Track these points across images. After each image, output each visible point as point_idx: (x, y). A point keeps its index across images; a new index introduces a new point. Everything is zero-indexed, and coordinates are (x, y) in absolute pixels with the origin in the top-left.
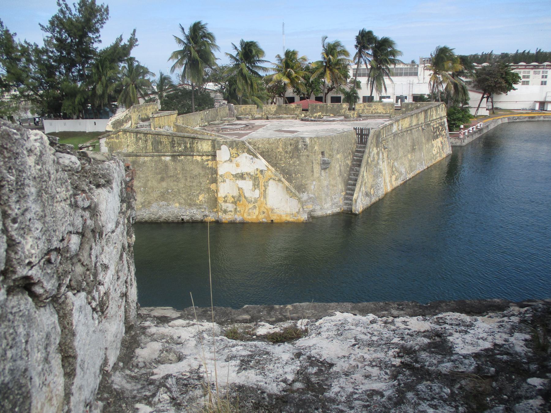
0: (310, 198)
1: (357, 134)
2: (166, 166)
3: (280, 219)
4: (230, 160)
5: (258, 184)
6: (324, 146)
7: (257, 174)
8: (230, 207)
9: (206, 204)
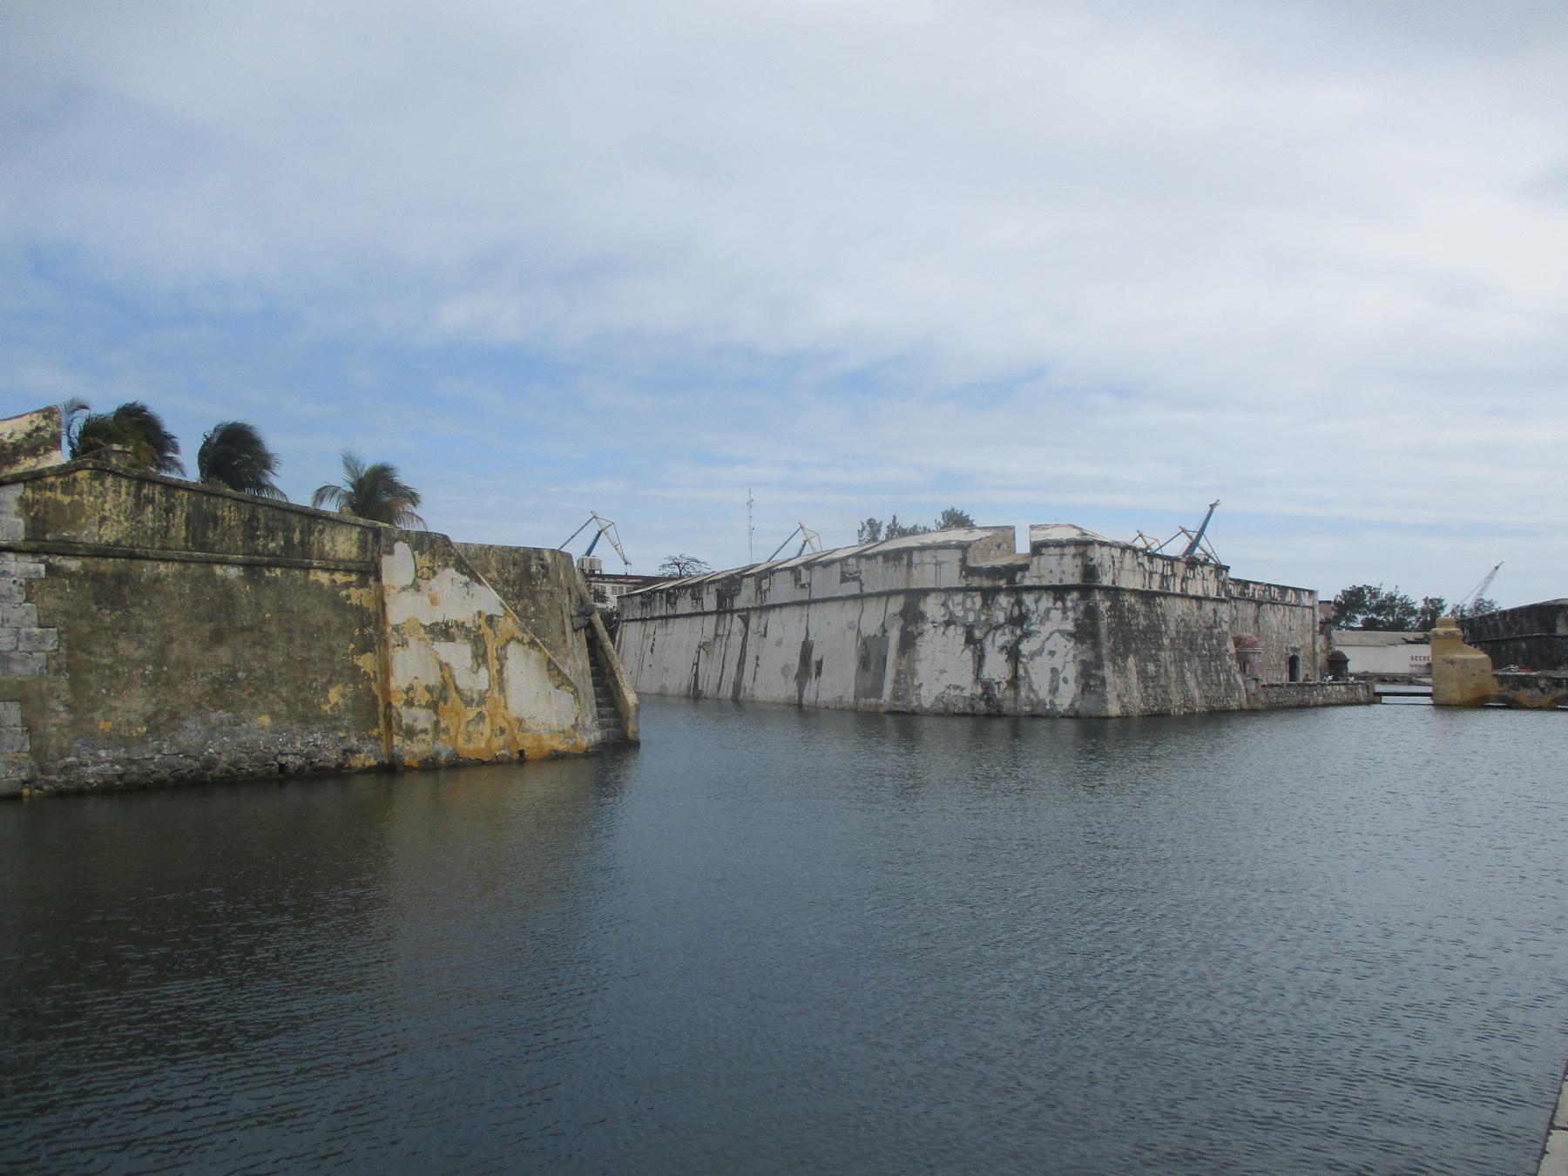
2: (228, 594)
4: (415, 586)
9: (349, 716)
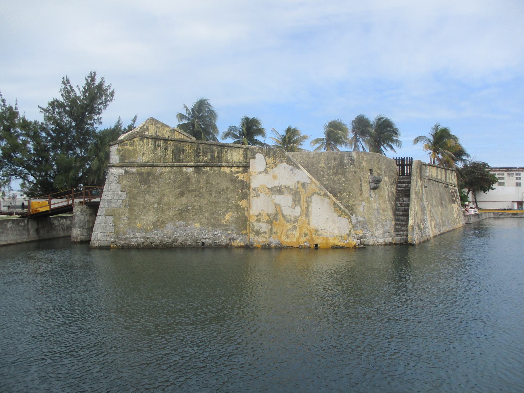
0: (359, 222)
1: (397, 165)
3: (327, 243)
4: (266, 171)
6: (373, 163)
7: (298, 188)
8: (264, 227)
9: (234, 225)
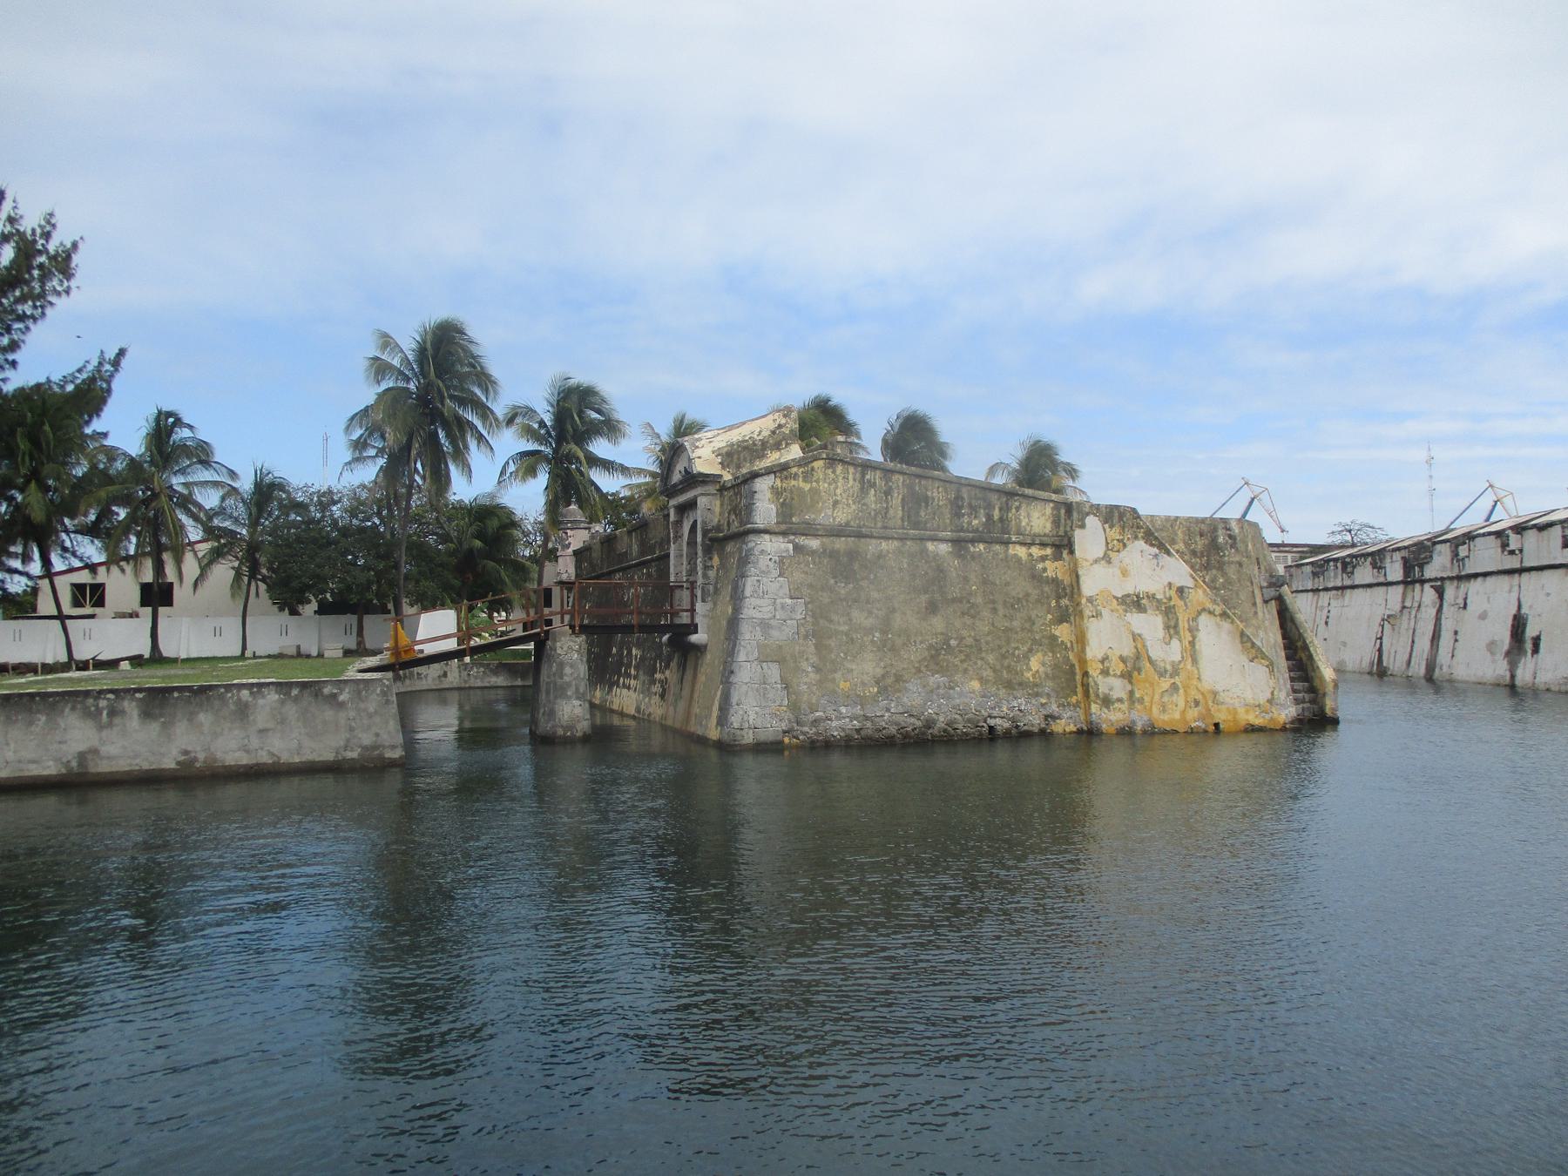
4: (1107, 559)
5: (1176, 627)
8: (1118, 688)
9: (1049, 683)
